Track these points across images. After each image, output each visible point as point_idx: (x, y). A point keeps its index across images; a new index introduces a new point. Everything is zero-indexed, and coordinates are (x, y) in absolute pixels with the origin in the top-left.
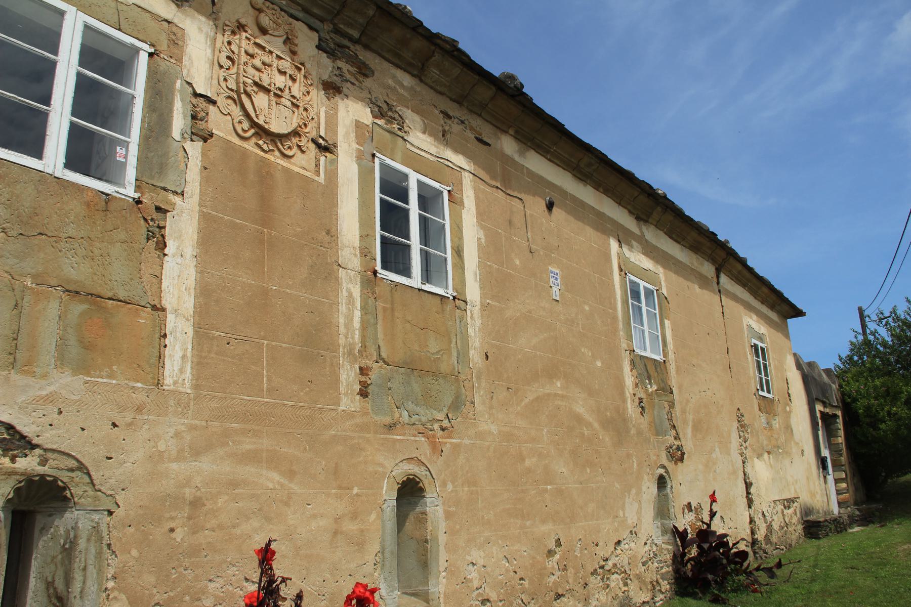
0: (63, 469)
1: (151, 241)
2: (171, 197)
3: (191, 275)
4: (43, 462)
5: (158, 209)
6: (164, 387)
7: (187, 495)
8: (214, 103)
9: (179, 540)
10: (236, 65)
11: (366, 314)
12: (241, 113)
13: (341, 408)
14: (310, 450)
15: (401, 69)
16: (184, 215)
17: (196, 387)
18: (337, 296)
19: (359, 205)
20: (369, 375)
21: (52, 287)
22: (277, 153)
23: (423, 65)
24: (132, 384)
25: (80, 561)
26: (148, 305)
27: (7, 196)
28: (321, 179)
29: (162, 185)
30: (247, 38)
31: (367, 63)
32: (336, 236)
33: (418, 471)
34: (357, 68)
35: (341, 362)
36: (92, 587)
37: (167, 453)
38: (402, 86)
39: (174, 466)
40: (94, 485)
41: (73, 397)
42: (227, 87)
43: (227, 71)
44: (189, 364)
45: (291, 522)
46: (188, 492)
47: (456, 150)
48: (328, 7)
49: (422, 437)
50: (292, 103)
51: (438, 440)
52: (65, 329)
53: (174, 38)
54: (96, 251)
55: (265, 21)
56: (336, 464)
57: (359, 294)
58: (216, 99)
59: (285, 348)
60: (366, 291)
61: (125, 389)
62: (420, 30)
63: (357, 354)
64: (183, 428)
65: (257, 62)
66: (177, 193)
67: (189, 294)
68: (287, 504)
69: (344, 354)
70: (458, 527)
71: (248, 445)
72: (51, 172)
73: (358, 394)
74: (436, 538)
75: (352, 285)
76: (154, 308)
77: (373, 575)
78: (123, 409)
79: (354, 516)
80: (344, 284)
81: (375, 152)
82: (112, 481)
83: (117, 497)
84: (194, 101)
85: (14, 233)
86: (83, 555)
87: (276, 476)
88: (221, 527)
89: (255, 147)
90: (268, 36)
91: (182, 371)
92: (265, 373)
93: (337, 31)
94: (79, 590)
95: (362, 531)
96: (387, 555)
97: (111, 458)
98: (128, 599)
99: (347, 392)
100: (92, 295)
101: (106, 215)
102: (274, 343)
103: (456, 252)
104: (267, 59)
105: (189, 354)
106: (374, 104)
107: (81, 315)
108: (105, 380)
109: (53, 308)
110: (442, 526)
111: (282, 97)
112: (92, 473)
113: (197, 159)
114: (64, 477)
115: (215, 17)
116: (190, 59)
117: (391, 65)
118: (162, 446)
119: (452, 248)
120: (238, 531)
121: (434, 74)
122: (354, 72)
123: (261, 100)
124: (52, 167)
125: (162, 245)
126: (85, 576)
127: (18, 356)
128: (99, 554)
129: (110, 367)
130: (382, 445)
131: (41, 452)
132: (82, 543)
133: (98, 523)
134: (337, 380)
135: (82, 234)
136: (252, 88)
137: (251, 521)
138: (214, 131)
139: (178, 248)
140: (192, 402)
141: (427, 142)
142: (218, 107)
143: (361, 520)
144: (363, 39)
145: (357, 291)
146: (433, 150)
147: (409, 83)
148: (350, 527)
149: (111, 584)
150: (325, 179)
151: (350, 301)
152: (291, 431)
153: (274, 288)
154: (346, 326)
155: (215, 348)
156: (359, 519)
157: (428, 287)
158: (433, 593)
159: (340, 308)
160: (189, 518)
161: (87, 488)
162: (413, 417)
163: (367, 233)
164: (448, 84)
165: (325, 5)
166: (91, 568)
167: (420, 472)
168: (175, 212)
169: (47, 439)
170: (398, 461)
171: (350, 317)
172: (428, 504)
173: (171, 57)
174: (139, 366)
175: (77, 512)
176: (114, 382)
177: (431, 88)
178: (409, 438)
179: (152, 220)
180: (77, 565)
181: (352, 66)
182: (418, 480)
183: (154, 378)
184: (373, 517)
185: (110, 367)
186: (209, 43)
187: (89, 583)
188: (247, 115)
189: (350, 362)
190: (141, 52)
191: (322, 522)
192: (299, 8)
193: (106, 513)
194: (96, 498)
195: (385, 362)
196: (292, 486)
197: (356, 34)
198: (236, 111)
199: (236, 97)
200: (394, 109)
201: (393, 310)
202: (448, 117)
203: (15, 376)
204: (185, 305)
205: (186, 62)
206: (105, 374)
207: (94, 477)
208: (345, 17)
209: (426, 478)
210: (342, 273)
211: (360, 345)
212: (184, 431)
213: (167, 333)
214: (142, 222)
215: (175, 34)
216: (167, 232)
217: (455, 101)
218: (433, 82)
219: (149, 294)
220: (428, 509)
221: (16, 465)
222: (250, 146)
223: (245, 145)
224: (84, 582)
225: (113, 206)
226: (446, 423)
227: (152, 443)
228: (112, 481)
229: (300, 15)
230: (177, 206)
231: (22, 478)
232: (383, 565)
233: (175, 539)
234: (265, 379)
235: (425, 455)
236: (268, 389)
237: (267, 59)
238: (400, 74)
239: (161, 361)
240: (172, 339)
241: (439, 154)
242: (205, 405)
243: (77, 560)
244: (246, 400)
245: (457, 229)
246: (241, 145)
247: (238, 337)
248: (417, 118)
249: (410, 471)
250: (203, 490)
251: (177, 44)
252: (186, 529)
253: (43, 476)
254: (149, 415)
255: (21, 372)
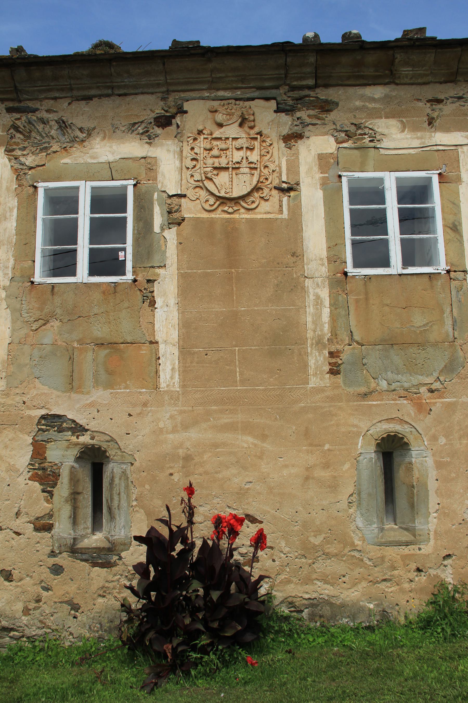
0: (103, 441)
1: (145, 302)
2: (157, 270)
3: (175, 316)
4: (92, 438)
5: (149, 281)
6: (161, 389)
7: (181, 454)
8: (185, 196)
9: (176, 480)
10: (199, 162)
11: (336, 309)
12: (207, 194)
13: (310, 386)
14: (280, 420)
15: (370, 85)
16: (167, 279)
17: (183, 386)
18: (304, 301)
19: (325, 223)
20: (339, 357)
21: (88, 344)
22: (242, 210)
23: (391, 71)
24: (138, 390)
25: (117, 490)
26: (147, 342)
27: (60, 302)
28: (285, 214)
29: (150, 265)
31: (329, 99)
32: (302, 255)
33: (400, 429)
34: (319, 109)
35: (309, 351)
36: (124, 504)
37: (165, 429)
38: (373, 100)
39: (171, 436)
40: (121, 449)
41: (105, 402)
42: (195, 181)
44: (177, 373)
45: (264, 470)
46: (181, 452)
47: (447, 130)
48: (275, 76)
49: (404, 400)
50: (251, 168)
51: (424, 401)
52: (97, 366)
53: (149, 166)
54: (111, 318)
55: (220, 117)
56: (306, 428)
57: (328, 295)
58: (185, 193)
59: (254, 350)
60: (334, 291)
61: (135, 394)
62: (368, 46)
63: (327, 342)
64: (176, 413)
65: (215, 152)
66: (162, 267)
67: (175, 329)
68: (260, 458)
69: (312, 344)
70: (453, 475)
71: (226, 419)
72: (81, 282)
73: (328, 373)
74: (425, 486)
75: (320, 290)
76: (151, 343)
77: (348, 511)
78: (134, 405)
79: (326, 466)
80: (311, 290)
81: (340, 173)
82: (131, 447)
83: (135, 455)
84: (169, 201)
85: (65, 321)
86: (118, 487)
87: (250, 439)
88: (206, 473)
89: (222, 213)
91: (172, 378)
92: (238, 370)
93: (293, 88)
94: (117, 505)
95: (335, 477)
96: (364, 495)
97: (129, 434)
98: (145, 512)
99: (316, 373)
100: (111, 343)
101: (115, 295)
102: (244, 348)
103: (451, 229)
104: (221, 145)
105: (177, 366)
106: (340, 131)
107: (106, 356)
108: (122, 391)
109: (90, 356)
110: (433, 474)
112: (119, 443)
113: (174, 239)
114: (104, 446)
116: (162, 175)
117: (357, 88)
118: (161, 425)
119: (445, 226)
120: (220, 476)
121: (406, 72)
122: (316, 114)
123: (223, 178)
124: (81, 279)
125: (153, 303)
126: (120, 498)
127: (74, 384)
128: (127, 487)
129: (125, 382)
130: (356, 410)
131: (91, 432)
132: (117, 481)
133: (125, 470)
134: (306, 366)
135: (102, 310)
136: (212, 174)
137: (230, 469)
139: (164, 302)
140: (181, 396)
141: (407, 138)
143: (334, 469)
144: (319, 82)
145: (325, 294)
146: (416, 143)
147: (382, 93)
148: (320, 473)
149: (134, 503)
150: (288, 215)
151: (318, 302)
152: (263, 407)
153: (243, 309)
154: (314, 322)
155: (196, 359)
156: (332, 468)
157: (411, 270)
158: (421, 530)
159: (307, 310)
160: (183, 467)
161: (117, 451)
162: (393, 384)
163: (335, 243)
164: (429, 72)
165: (272, 76)
166: (122, 494)
167: (403, 430)
168: (159, 280)
169: (92, 426)
170: (375, 422)
171: (318, 316)
172: (413, 456)
173: (149, 180)
174: (143, 379)
175: (112, 464)
176: (128, 391)
177: (412, 84)
178: (387, 402)
179: (145, 289)
180: (115, 491)
181: (313, 110)
182: (401, 436)
183: (153, 385)
184: (347, 466)
185: (125, 382)
186: (176, 156)
187: (122, 502)
188: (212, 194)
189: (318, 350)
190: (129, 187)
191: (293, 471)
193: (130, 464)
194: (122, 456)
195: (358, 343)
196: (265, 445)
197: (311, 82)
198: (203, 193)
199: (201, 185)
200: (363, 126)
201: (367, 299)
202: (439, 101)
203: (73, 395)
204: (172, 337)
205: (160, 178)
206: (122, 387)
207: (120, 445)
208: (293, 76)
209: (411, 434)
210: (308, 283)
211: (330, 335)
212: (176, 415)
213: (160, 356)
214: (138, 292)
215: (150, 163)
216: (155, 294)
217: (445, 82)
218: (411, 78)
219: (147, 335)
220: (413, 460)
221: (79, 440)
222: (218, 215)
223: (213, 215)
224: (119, 501)
225: (118, 289)
226: (437, 385)
227: (155, 423)
228: (131, 447)
229: (256, 94)
230: (161, 275)
231: (82, 446)
232: (360, 503)
233: (173, 480)
234: (238, 374)
235: (409, 415)
236: (240, 380)
237: (223, 146)
238: (369, 91)
239: (158, 374)
240: (163, 359)
241: (424, 143)
242: (190, 397)
243: (115, 489)
244: (223, 390)
245: (451, 206)
246: (209, 216)
247: (214, 349)
248: (393, 122)
249: (390, 429)
250: (192, 450)
251: (152, 169)
252: (181, 474)
253: (93, 445)
254: (151, 407)
255: (77, 392)
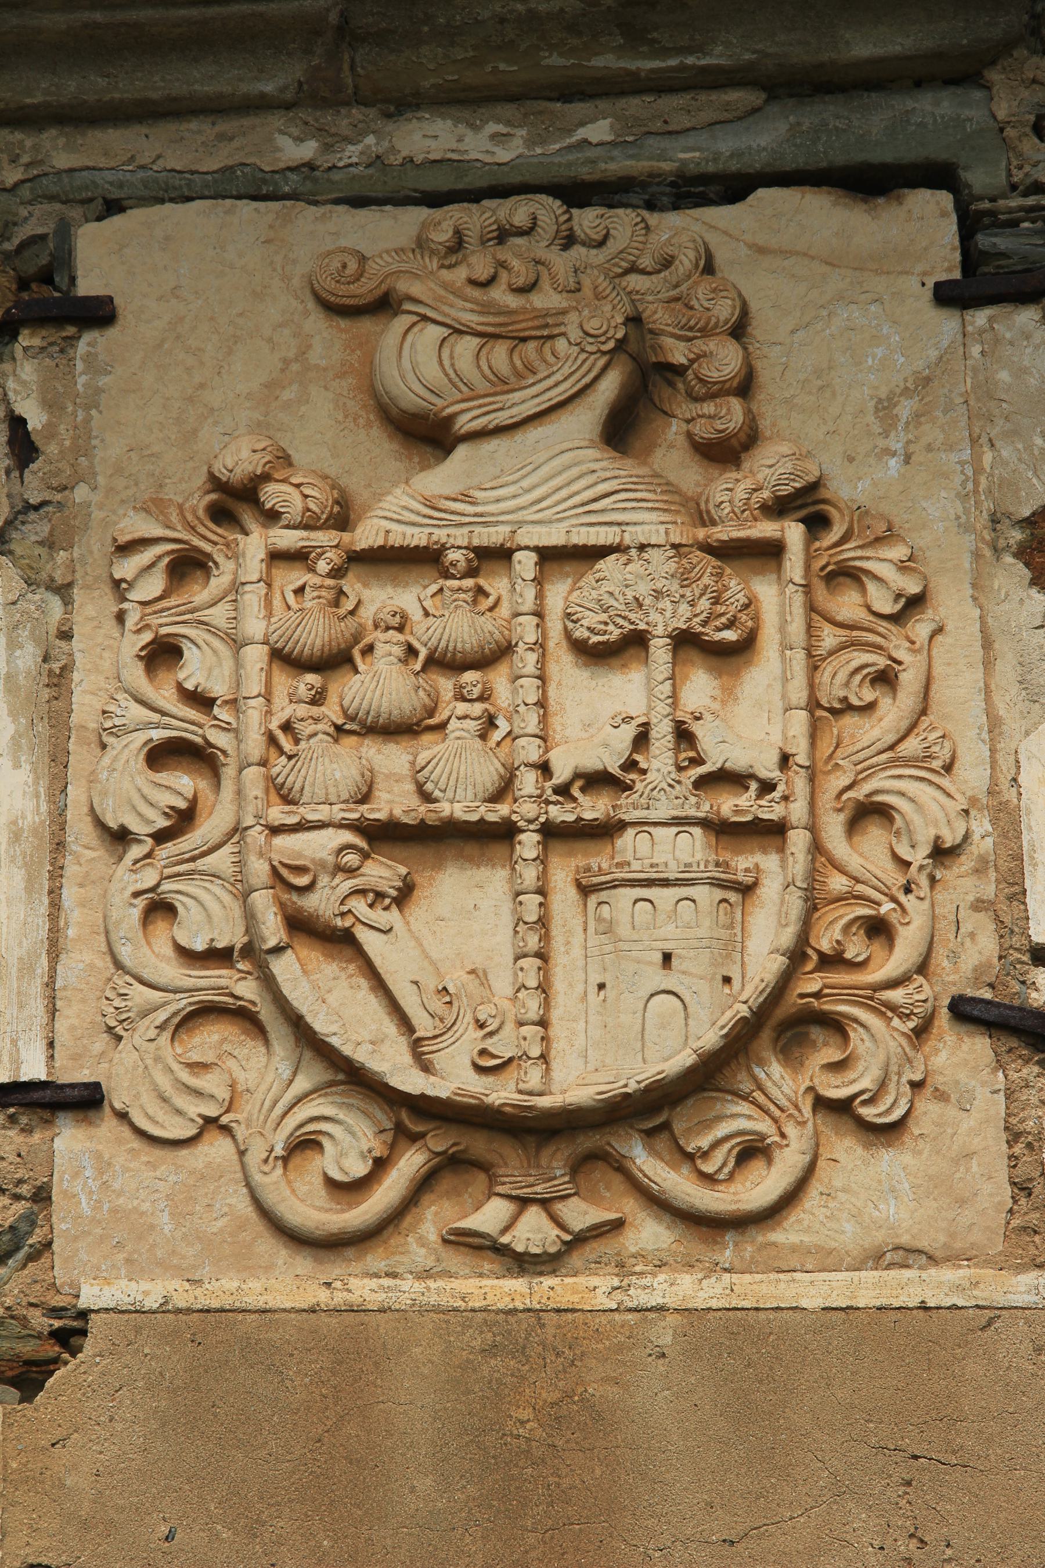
10: (228, 772)
12: (302, 1084)
30: (277, 557)
43: (170, 849)
89: (454, 1260)
90: (462, 451)
111: (622, 826)
115: (44, 529)
138: (90, 1296)
142: (123, 1116)
192: (734, 96)
199: (248, 990)
